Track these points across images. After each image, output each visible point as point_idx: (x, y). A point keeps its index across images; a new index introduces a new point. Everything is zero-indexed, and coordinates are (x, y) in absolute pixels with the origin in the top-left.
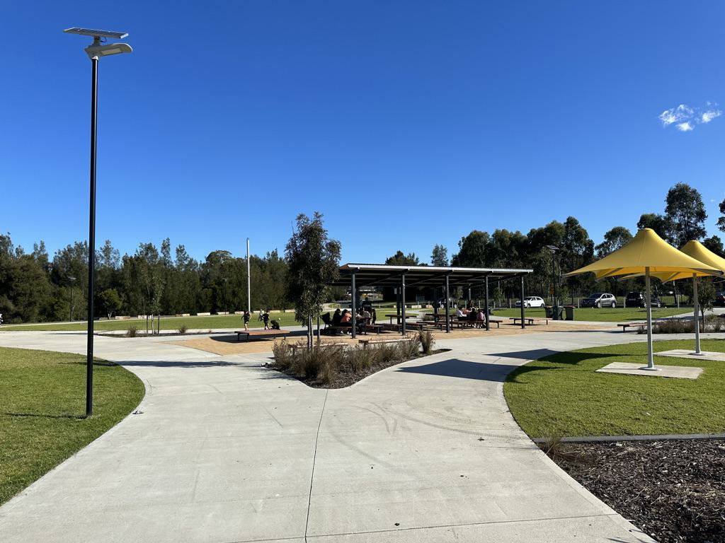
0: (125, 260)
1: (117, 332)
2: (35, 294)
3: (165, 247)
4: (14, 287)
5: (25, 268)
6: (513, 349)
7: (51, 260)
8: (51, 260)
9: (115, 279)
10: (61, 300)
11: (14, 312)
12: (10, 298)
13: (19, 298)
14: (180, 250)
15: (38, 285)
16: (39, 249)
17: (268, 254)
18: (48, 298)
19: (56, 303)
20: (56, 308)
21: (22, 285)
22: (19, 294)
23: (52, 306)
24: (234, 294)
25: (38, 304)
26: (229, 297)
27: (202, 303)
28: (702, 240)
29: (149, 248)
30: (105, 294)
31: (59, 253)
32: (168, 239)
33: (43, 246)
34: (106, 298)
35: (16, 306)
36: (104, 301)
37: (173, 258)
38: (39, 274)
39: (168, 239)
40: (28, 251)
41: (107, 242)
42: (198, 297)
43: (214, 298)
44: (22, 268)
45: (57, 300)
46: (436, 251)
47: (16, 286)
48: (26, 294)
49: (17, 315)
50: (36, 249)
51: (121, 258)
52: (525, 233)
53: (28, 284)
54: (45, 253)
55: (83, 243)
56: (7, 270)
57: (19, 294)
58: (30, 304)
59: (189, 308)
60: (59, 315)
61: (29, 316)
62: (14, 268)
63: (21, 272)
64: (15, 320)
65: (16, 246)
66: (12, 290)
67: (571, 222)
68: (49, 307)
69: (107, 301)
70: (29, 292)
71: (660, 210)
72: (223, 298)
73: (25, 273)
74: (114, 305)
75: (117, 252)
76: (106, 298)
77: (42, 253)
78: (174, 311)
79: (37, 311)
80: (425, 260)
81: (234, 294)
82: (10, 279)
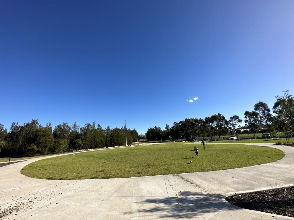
0: (81, 129)
1: (18, 161)
2: (48, 142)
3: (94, 125)
4: (38, 140)
5: (44, 131)
6: (18, 164)
7: (53, 129)
8: (53, 129)
9: (78, 136)
10: (58, 144)
11: (37, 151)
12: (35, 145)
13: (40, 144)
14: (99, 126)
15: (49, 138)
16: (48, 125)
17: (123, 127)
18: (53, 144)
19: (56, 146)
20: (56, 148)
21: (42, 139)
22: (40, 143)
23: (54, 147)
24: (117, 140)
25: (48, 147)
26: (116, 141)
27: (107, 143)
28: (13, 148)
29: (89, 125)
30: (76, 141)
31: (57, 127)
32: (95, 122)
33: (50, 124)
34: (77, 143)
35: (38, 148)
36: (76, 144)
37: (96, 127)
38: (50, 134)
39: (95, 122)
40: (44, 126)
41: (75, 123)
42: (106, 141)
43: (111, 141)
44: (43, 131)
45: (56, 145)
46: (166, 126)
47: (39, 139)
48: (43, 143)
49: (38, 152)
50: (47, 125)
51: (80, 128)
52: (210, 117)
53: (45, 138)
54: (51, 127)
55: (66, 123)
56: (35, 132)
57: (40, 143)
58: (45, 147)
59: (103, 145)
60: (57, 151)
61: (43, 152)
62: (39, 132)
63: (42, 133)
64: (37, 154)
65: (39, 124)
66: (37, 141)
67: (219, 115)
68: (53, 148)
69: (77, 144)
70: (45, 141)
71: (251, 109)
72: (114, 141)
73: (44, 134)
74: (80, 145)
75: (79, 126)
76: (77, 143)
77: (49, 127)
78: (98, 147)
79: (47, 149)
80: (163, 128)
81: (117, 140)
82: (36, 136)
